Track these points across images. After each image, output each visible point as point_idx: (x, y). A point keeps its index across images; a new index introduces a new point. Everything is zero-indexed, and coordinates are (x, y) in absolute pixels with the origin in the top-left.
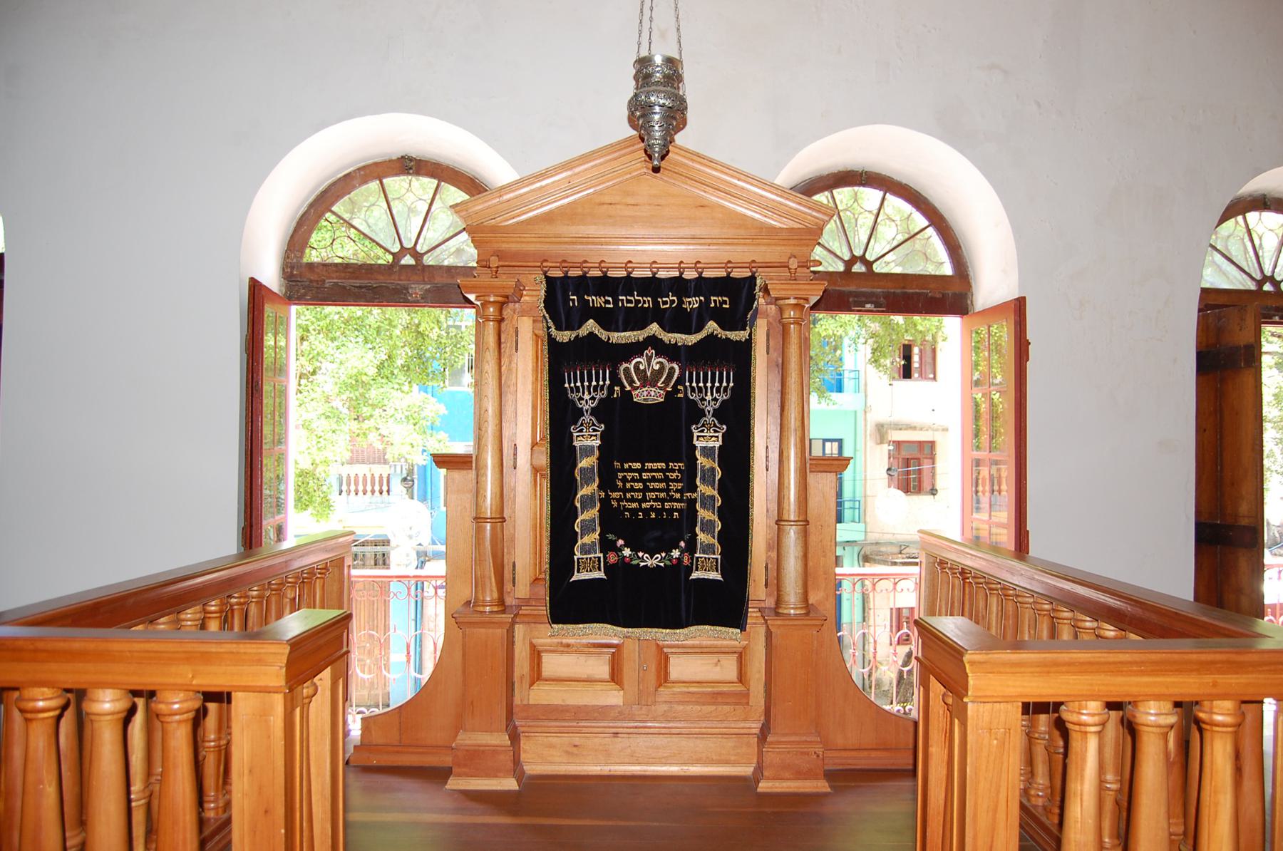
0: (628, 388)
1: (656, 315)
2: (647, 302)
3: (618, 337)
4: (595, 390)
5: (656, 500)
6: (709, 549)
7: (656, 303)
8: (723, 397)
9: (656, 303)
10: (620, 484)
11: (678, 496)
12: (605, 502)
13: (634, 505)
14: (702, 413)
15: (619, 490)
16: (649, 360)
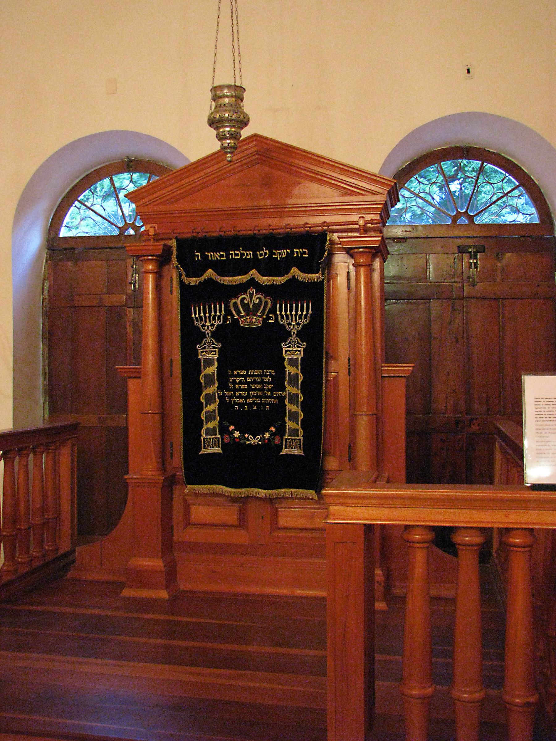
0: (237, 317)
1: (255, 263)
2: (249, 255)
3: (226, 280)
4: (300, 318)
5: (257, 397)
6: (295, 432)
7: (255, 255)
8: (217, 323)
9: (255, 255)
10: (231, 386)
11: (269, 394)
12: (222, 398)
13: (241, 401)
14: (289, 334)
15: (231, 390)
16: (251, 296)
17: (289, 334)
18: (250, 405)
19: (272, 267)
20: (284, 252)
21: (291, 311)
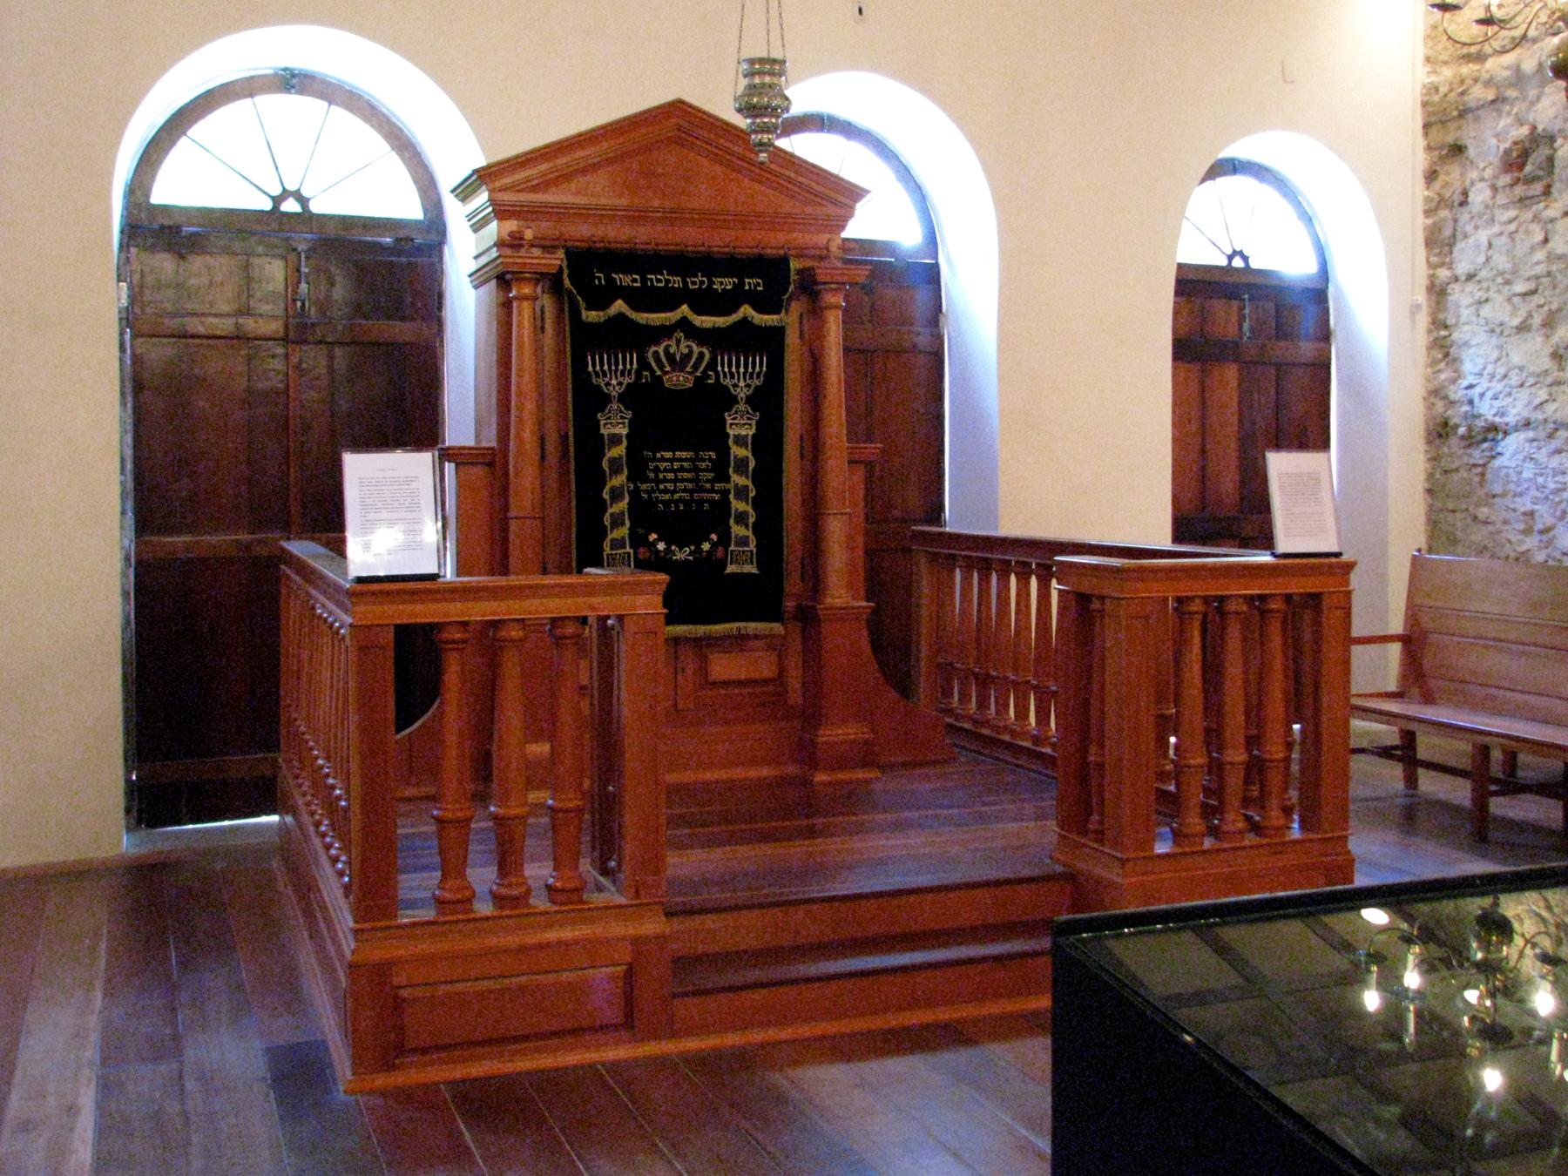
2: (676, 282)
3: (643, 318)
4: (623, 374)
5: (685, 490)
6: (743, 541)
8: (626, 381)
9: (685, 283)
10: (652, 475)
11: (708, 486)
12: (634, 494)
13: (667, 497)
15: (651, 481)
16: (678, 341)
17: (735, 400)
18: (677, 502)
19: (707, 302)
20: (728, 283)
21: (738, 367)
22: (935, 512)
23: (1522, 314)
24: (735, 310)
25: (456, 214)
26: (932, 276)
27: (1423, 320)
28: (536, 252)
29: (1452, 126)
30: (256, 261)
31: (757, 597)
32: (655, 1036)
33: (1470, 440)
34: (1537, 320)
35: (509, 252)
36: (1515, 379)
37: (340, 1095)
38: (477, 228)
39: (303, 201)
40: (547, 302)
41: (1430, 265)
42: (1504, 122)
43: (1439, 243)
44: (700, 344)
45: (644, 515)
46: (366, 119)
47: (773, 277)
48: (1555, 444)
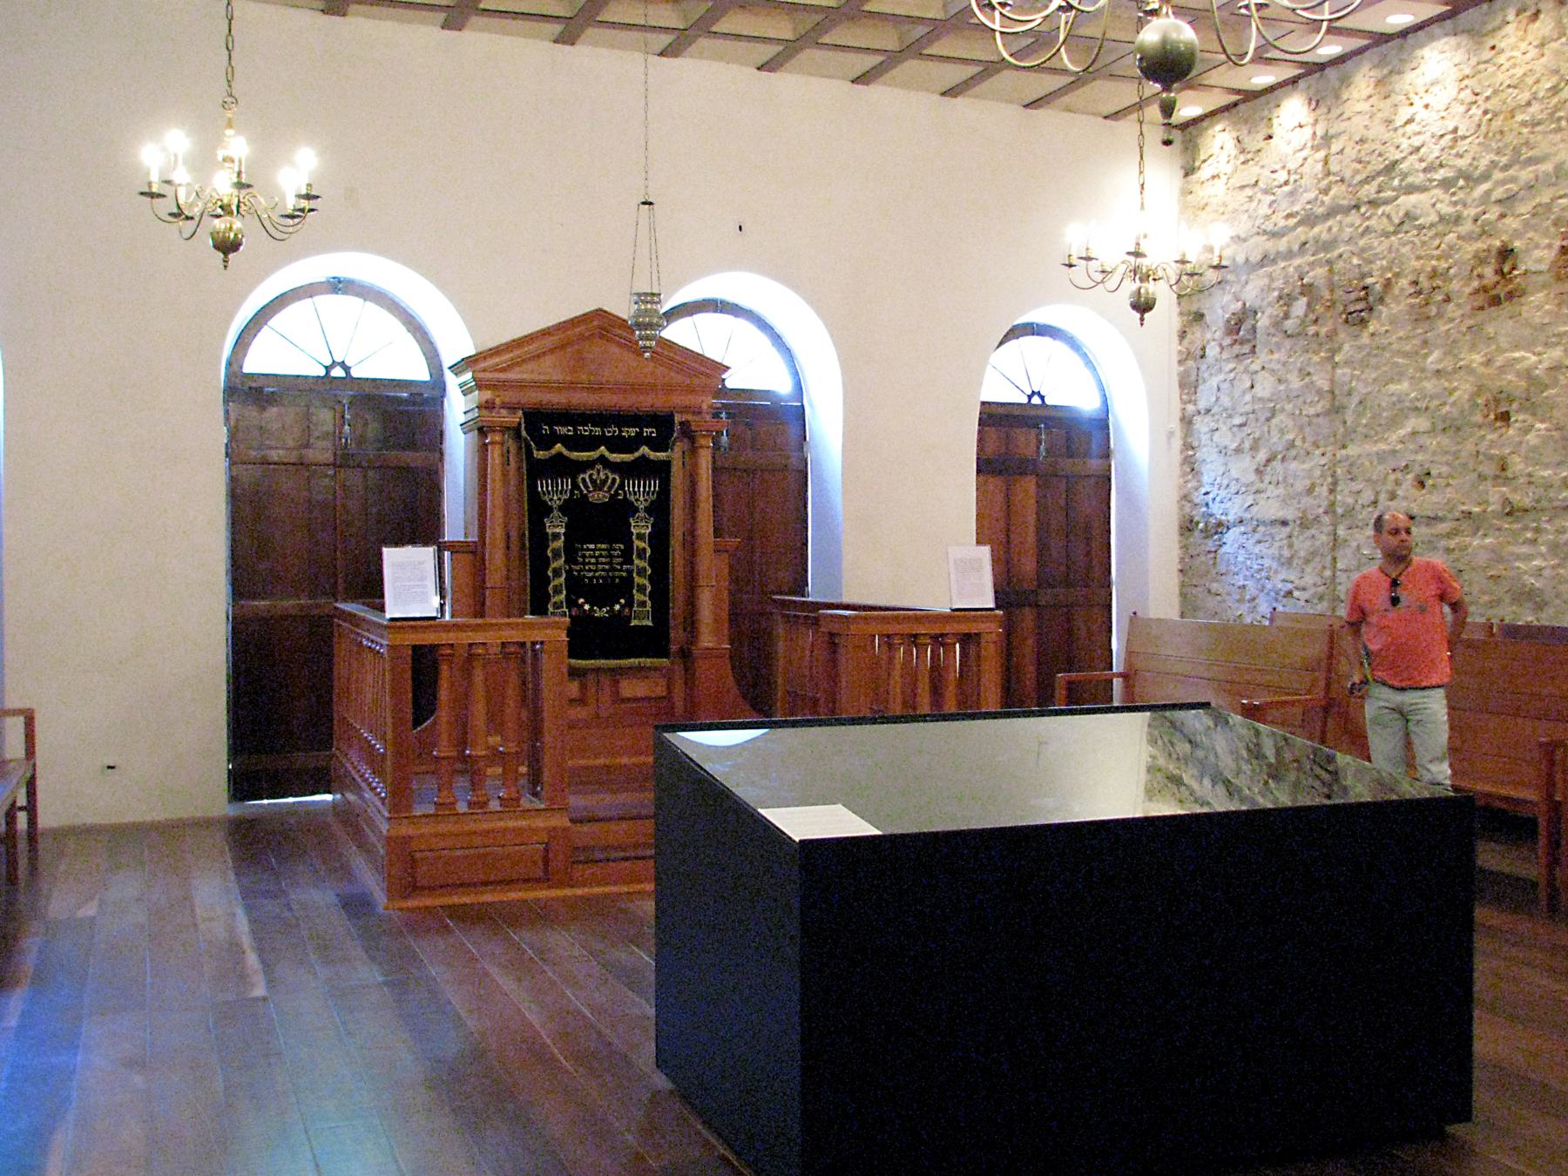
2: (597, 431)
3: (575, 455)
6: (643, 604)
17: (637, 510)
19: (617, 445)
20: (633, 431)
22: (800, 585)
23: (1238, 440)
24: (637, 449)
25: (452, 382)
26: (800, 413)
27: (1177, 443)
28: (504, 412)
29: (1194, 298)
30: (312, 410)
31: (653, 642)
32: (560, 884)
33: (1207, 533)
34: (1247, 445)
35: (485, 412)
36: (1233, 489)
37: (380, 909)
38: (465, 393)
39: (347, 369)
40: (512, 445)
41: (1184, 402)
42: (1227, 298)
43: (1189, 386)
44: (613, 472)
45: (576, 586)
46: (390, 310)
47: (662, 426)
48: (1257, 536)
